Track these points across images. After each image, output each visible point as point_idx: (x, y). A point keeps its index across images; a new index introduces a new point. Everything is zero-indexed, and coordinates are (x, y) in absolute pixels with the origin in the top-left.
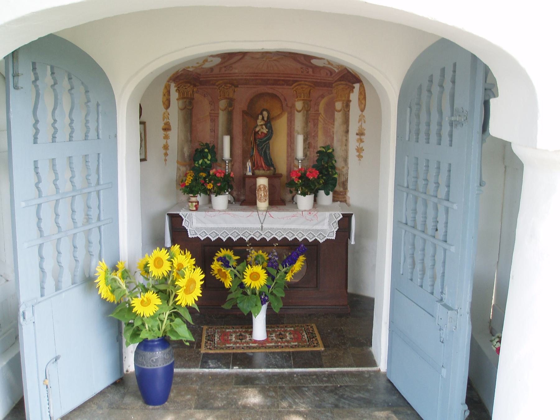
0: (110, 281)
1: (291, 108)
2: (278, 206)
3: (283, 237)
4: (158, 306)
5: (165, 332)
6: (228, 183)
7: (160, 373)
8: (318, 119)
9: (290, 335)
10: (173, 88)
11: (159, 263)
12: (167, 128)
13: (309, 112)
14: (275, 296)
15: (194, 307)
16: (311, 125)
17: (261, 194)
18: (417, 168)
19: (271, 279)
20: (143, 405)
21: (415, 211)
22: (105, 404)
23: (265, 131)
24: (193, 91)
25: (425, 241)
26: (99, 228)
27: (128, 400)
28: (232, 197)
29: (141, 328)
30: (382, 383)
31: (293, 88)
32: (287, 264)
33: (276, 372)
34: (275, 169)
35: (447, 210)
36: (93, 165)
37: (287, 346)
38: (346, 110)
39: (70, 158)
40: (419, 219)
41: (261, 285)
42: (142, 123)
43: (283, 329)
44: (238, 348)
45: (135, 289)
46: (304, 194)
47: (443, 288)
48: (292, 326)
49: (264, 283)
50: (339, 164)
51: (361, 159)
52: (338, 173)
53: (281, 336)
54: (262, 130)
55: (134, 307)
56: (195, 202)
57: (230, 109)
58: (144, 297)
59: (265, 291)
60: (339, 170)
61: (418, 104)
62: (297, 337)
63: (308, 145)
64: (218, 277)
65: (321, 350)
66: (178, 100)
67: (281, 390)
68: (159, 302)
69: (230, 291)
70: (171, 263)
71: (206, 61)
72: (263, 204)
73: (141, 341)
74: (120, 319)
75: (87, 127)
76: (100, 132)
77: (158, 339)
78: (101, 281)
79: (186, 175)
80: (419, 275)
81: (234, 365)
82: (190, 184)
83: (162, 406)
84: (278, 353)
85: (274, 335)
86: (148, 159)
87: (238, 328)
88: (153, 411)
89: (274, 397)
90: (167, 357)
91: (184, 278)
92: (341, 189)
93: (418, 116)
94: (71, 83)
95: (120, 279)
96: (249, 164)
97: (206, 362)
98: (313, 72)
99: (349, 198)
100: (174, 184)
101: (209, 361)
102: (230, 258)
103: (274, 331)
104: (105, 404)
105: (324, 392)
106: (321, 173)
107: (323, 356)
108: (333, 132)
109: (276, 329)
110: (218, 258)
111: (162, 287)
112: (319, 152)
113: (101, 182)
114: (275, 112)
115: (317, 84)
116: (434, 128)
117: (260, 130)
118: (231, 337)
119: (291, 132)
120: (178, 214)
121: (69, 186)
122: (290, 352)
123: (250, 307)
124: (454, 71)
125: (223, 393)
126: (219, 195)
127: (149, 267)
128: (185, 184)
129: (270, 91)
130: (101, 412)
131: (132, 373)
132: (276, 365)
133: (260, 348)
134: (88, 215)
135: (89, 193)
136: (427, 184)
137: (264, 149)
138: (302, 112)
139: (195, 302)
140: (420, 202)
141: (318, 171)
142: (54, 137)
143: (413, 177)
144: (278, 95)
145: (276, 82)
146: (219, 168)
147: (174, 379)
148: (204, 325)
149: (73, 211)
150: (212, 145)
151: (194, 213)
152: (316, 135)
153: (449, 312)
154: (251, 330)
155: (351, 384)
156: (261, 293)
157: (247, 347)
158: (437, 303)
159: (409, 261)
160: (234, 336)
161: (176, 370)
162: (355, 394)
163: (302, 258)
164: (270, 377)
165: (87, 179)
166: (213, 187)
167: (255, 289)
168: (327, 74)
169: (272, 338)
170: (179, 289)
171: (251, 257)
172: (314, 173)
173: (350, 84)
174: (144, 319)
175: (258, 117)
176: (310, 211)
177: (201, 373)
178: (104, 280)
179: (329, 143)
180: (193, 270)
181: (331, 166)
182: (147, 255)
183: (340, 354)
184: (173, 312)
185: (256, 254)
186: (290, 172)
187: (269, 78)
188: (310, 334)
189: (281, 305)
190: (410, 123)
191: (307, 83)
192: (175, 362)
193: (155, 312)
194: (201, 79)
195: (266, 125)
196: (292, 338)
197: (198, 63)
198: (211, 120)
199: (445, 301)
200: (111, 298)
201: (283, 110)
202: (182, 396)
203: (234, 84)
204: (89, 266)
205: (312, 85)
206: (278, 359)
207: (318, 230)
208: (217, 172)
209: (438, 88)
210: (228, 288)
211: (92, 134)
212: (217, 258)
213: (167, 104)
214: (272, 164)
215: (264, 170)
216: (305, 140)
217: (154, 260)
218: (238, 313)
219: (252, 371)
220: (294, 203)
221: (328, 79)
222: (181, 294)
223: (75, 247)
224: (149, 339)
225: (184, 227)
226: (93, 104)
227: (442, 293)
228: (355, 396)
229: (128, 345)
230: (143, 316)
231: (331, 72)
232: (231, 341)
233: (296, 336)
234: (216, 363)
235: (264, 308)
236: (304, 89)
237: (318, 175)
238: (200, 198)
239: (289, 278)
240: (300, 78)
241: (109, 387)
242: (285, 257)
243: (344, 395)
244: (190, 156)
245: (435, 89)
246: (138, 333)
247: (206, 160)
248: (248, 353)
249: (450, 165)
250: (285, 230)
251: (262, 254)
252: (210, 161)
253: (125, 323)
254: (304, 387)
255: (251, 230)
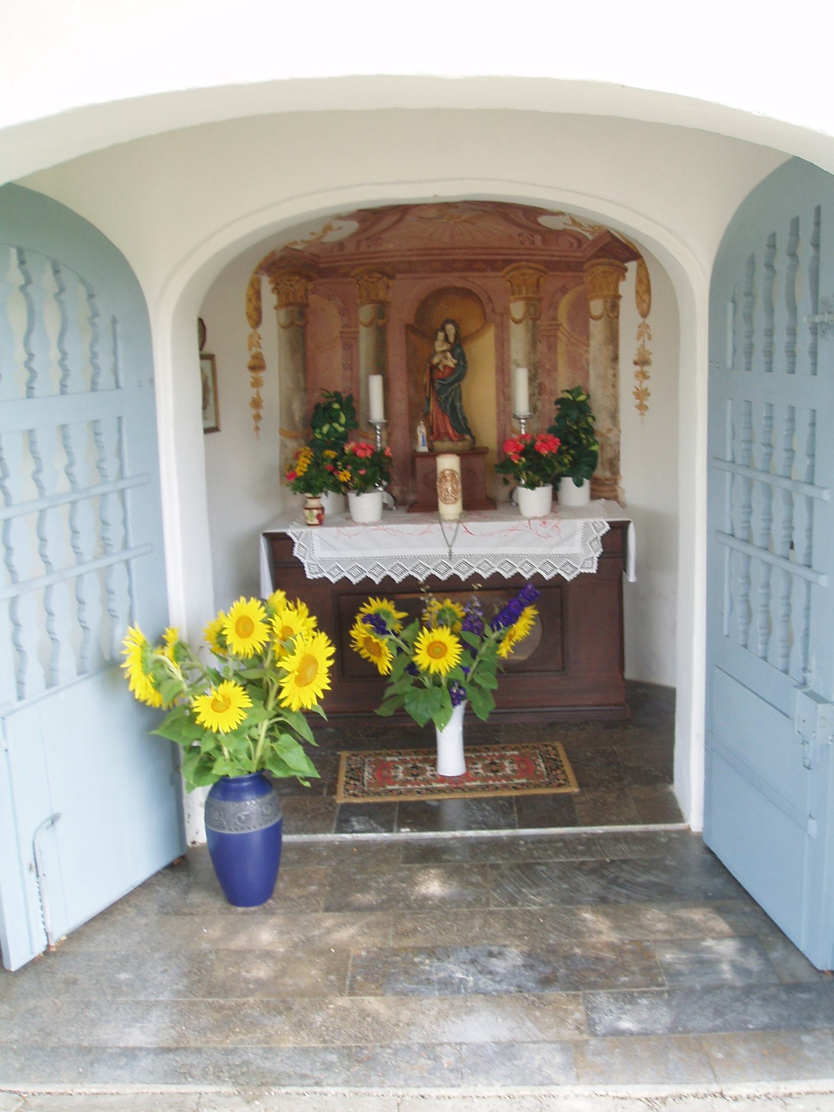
0: (150, 666)
1: (502, 315)
2: (480, 511)
3: (493, 571)
4: (245, 710)
5: (262, 762)
6: (381, 468)
7: (256, 843)
8: (556, 336)
9: (511, 765)
10: (266, 285)
11: (245, 627)
12: (257, 365)
13: (539, 322)
14: (479, 687)
15: (315, 710)
16: (542, 347)
17: (447, 489)
18: (750, 423)
19: (469, 655)
20: (225, 906)
21: (748, 509)
22: (151, 907)
23: (451, 362)
24: (306, 290)
25: (769, 566)
26: (127, 562)
27: (196, 897)
28: (391, 497)
29: (215, 754)
30: (696, 851)
31: (504, 277)
32: (501, 624)
33: (483, 837)
34: (473, 437)
35: (810, 503)
36: (108, 440)
37: (505, 787)
38: (612, 315)
39: (63, 427)
40: (758, 525)
41: (450, 667)
42: (206, 357)
43: (497, 754)
44: (410, 791)
45: (200, 679)
46: (532, 485)
47: (806, 660)
48: (516, 747)
49: (456, 663)
50: (601, 424)
51: (645, 412)
52: (599, 443)
53: (494, 767)
54: (445, 362)
55: (198, 713)
56: (317, 509)
57: (380, 322)
58: (217, 693)
59: (458, 678)
60: (602, 435)
61: (749, 294)
62: (526, 768)
63: (537, 388)
64: (365, 654)
65: (574, 792)
66: (276, 308)
67: (495, 872)
68: (247, 703)
69: (389, 681)
70: (268, 626)
71: (328, 228)
72: (450, 509)
73: (216, 780)
74: (174, 739)
75: (96, 367)
76: (121, 376)
77: (249, 776)
78: (133, 666)
79: (297, 456)
80: (759, 636)
81: (402, 824)
82: (305, 473)
83: (261, 907)
84: (488, 800)
85: (479, 766)
86: (222, 427)
87: (408, 754)
88: (245, 917)
89: (480, 885)
90: (267, 810)
91: (294, 654)
92: (608, 474)
93: (749, 318)
94: (58, 280)
95: (171, 661)
96: (422, 431)
97: (347, 821)
98: (544, 241)
99: (623, 491)
100: (276, 476)
101: (353, 819)
102: (388, 614)
103: (480, 758)
104: (151, 907)
105: (579, 873)
106: (564, 442)
107: (578, 803)
108: (587, 360)
109: (484, 755)
110: (365, 617)
111: (253, 675)
112: (560, 401)
113: (128, 473)
114: (471, 325)
115: (552, 266)
116: (781, 339)
117: (441, 361)
118: (397, 771)
119: (503, 364)
120: (285, 534)
121: (62, 484)
122: (510, 797)
123: (430, 712)
124: (818, 224)
125: (380, 880)
126: (364, 492)
127: (226, 635)
128: (295, 473)
129: (459, 284)
130: (143, 921)
131: (202, 847)
132: (484, 823)
133: (452, 791)
134: (103, 538)
135: (104, 495)
136: (770, 454)
137: (450, 400)
138: (524, 322)
139: (318, 703)
140: (758, 491)
141: (558, 440)
142: (30, 388)
143: (744, 441)
144: (474, 290)
145: (470, 266)
146: (362, 441)
147: (282, 854)
148: (343, 749)
149: (75, 532)
150: (347, 394)
151: (316, 531)
152: (554, 368)
153: (821, 706)
154: (435, 757)
155: (632, 857)
156: (451, 683)
157: (427, 789)
158: (796, 689)
159: (740, 609)
160: (401, 768)
161: (286, 838)
162: (639, 877)
163: (530, 612)
164: (475, 846)
165: (99, 468)
166: (351, 478)
167: (438, 675)
168: (571, 244)
169: (476, 771)
170: (284, 677)
171: (430, 612)
172: (551, 443)
173: (618, 263)
174: (219, 737)
175: (436, 334)
176: (544, 519)
177: (337, 843)
178: (140, 664)
179: (579, 382)
180: (311, 638)
181: (584, 429)
182: (221, 613)
183: (611, 798)
184: (277, 723)
185: (439, 606)
186: (504, 441)
187: (456, 257)
188: (551, 761)
189: (491, 706)
190: (734, 333)
191: (532, 265)
192: (284, 822)
193: (240, 723)
194: (321, 266)
195: (452, 351)
196: (515, 770)
197: (313, 234)
198: (343, 347)
199: (812, 686)
200: (155, 699)
201: (486, 320)
202: (300, 886)
203: (388, 272)
204: (111, 639)
205: (543, 268)
206: (489, 811)
207: (562, 557)
208: (359, 446)
209: (787, 261)
210: (386, 674)
211: (105, 379)
212: (363, 617)
213: (256, 318)
214: (466, 426)
215: (451, 440)
216: (532, 379)
217: (235, 621)
218: (410, 725)
219: (437, 837)
220: (514, 504)
221: (573, 254)
222: (289, 684)
223: (81, 602)
224: (232, 776)
225: (296, 558)
226: (104, 321)
227: (805, 669)
228: (640, 880)
229: (191, 788)
230: (218, 732)
231: (580, 240)
232: (396, 779)
233: (523, 766)
234: (366, 821)
235: (458, 712)
236: (526, 277)
237: (560, 447)
238: (327, 501)
239: (504, 650)
240: (518, 255)
241: (159, 872)
242: (497, 611)
243: (618, 877)
244: (304, 419)
245: (782, 262)
246: (209, 764)
247: (336, 425)
248: (429, 803)
249: (814, 412)
250: (495, 557)
251: (452, 606)
252: (345, 426)
253: (185, 748)
254: (539, 864)
255: (429, 559)
